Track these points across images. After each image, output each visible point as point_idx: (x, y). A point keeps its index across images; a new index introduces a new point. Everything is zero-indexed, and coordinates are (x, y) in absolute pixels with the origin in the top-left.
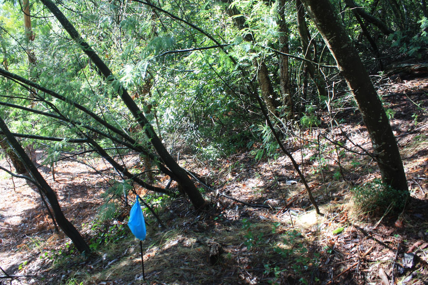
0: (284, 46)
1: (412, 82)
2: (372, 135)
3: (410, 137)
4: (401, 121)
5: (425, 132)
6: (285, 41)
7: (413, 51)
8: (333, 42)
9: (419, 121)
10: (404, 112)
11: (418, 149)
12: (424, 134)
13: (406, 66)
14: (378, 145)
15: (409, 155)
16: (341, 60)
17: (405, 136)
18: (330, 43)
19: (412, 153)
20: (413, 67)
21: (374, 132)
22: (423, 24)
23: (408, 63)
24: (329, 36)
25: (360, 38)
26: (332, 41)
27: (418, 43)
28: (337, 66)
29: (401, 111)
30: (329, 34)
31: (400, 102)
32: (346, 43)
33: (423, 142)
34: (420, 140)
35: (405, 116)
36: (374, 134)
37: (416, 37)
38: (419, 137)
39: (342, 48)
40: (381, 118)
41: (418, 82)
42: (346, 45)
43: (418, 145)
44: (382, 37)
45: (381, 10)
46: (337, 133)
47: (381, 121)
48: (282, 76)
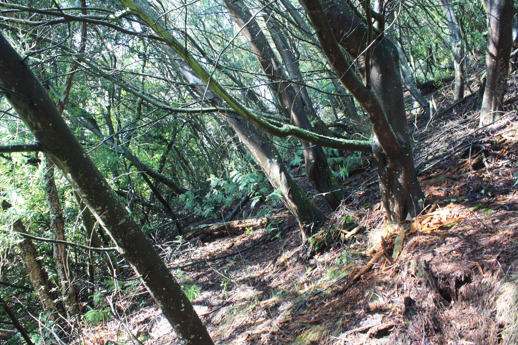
0: (57, 218)
1: (214, 244)
2: (176, 329)
3: (224, 311)
4: (211, 292)
5: (237, 302)
6: (57, 212)
7: (208, 212)
8: (106, 218)
9: (229, 289)
10: (212, 281)
11: (235, 325)
12: (237, 305)
13: (204, 227)
14: (186, 340)
15: (227, 335)
16: (120, 240)
17: (218, 310)
18: (104, 220)
19: (229, 330)
20: (211, 228)
21: (178, 325)
22: (212, 182)
23: (206, 223)
24: (100, 210)
25: (152, 200)
26: (104, 217)
27: (211, 202)
28: (117, 248)
29: (208, 281)
30: (100, 208)
31: (205, 270)
32: (123, 218)
33: (238, 316)
34: (235, 313)
35: (213, 285)
36: (178, 327)
37: (208, 196)
38: (233, 309)
39: (119, 224)
40: (183, 305)
41: (220, 243)
42: (124, 221)
43: (234, 320)
44: (176, 196)
45: (170, 166)
46: (139, 321)
47: (183, 310)
48: (58, 257)
